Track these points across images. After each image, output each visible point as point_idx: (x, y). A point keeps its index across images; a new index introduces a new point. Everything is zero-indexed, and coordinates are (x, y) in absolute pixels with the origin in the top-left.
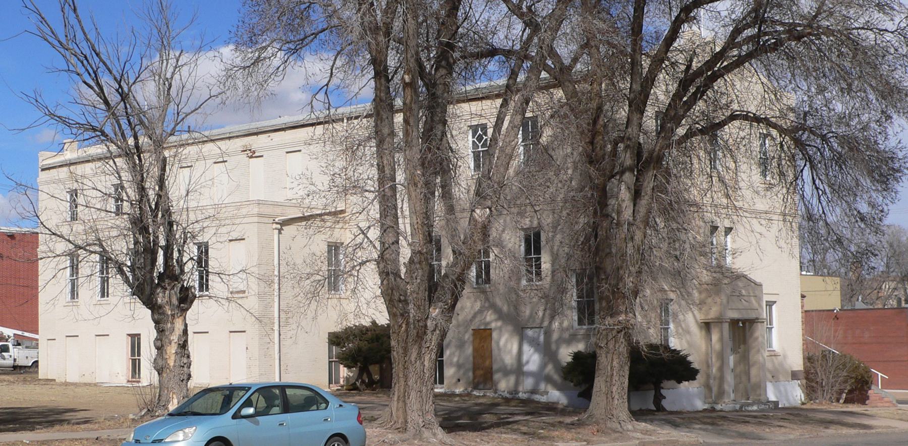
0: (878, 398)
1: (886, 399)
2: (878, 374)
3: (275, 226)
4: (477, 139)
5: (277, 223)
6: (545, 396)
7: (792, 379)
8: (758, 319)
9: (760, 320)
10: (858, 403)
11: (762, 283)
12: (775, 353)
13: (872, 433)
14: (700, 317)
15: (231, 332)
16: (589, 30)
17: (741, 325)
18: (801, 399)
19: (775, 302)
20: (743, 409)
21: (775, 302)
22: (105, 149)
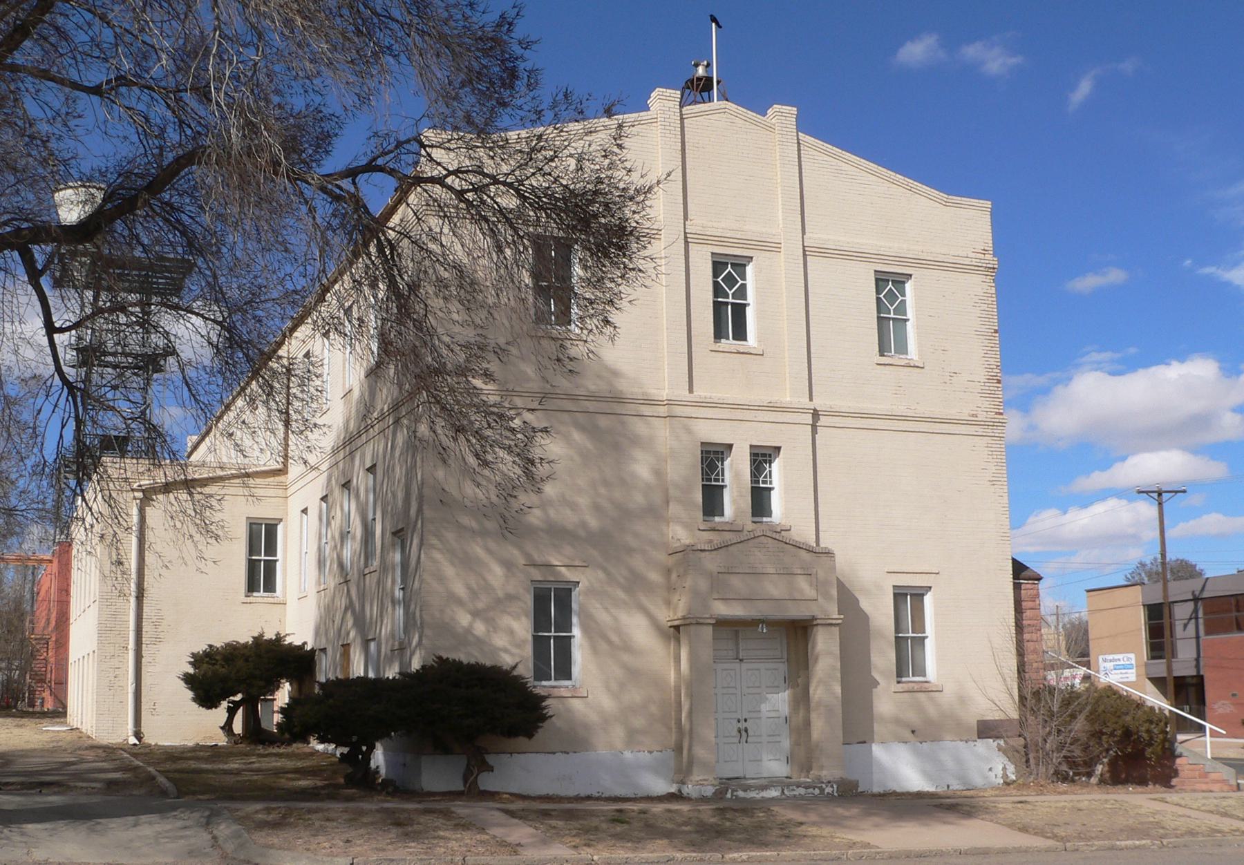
0: (1197, 773)
1: (1213, 776)
2: (1204, 727)
4: (738, 282)
7: (979, 738)
8: (816, 619)
9: (819, 622)
10: (1154, 784)
14: (666, 616)
16: (18, 192)
18: (1005, 776)
20: (729, 796)
21: (930, 588)
22: (658, 172)
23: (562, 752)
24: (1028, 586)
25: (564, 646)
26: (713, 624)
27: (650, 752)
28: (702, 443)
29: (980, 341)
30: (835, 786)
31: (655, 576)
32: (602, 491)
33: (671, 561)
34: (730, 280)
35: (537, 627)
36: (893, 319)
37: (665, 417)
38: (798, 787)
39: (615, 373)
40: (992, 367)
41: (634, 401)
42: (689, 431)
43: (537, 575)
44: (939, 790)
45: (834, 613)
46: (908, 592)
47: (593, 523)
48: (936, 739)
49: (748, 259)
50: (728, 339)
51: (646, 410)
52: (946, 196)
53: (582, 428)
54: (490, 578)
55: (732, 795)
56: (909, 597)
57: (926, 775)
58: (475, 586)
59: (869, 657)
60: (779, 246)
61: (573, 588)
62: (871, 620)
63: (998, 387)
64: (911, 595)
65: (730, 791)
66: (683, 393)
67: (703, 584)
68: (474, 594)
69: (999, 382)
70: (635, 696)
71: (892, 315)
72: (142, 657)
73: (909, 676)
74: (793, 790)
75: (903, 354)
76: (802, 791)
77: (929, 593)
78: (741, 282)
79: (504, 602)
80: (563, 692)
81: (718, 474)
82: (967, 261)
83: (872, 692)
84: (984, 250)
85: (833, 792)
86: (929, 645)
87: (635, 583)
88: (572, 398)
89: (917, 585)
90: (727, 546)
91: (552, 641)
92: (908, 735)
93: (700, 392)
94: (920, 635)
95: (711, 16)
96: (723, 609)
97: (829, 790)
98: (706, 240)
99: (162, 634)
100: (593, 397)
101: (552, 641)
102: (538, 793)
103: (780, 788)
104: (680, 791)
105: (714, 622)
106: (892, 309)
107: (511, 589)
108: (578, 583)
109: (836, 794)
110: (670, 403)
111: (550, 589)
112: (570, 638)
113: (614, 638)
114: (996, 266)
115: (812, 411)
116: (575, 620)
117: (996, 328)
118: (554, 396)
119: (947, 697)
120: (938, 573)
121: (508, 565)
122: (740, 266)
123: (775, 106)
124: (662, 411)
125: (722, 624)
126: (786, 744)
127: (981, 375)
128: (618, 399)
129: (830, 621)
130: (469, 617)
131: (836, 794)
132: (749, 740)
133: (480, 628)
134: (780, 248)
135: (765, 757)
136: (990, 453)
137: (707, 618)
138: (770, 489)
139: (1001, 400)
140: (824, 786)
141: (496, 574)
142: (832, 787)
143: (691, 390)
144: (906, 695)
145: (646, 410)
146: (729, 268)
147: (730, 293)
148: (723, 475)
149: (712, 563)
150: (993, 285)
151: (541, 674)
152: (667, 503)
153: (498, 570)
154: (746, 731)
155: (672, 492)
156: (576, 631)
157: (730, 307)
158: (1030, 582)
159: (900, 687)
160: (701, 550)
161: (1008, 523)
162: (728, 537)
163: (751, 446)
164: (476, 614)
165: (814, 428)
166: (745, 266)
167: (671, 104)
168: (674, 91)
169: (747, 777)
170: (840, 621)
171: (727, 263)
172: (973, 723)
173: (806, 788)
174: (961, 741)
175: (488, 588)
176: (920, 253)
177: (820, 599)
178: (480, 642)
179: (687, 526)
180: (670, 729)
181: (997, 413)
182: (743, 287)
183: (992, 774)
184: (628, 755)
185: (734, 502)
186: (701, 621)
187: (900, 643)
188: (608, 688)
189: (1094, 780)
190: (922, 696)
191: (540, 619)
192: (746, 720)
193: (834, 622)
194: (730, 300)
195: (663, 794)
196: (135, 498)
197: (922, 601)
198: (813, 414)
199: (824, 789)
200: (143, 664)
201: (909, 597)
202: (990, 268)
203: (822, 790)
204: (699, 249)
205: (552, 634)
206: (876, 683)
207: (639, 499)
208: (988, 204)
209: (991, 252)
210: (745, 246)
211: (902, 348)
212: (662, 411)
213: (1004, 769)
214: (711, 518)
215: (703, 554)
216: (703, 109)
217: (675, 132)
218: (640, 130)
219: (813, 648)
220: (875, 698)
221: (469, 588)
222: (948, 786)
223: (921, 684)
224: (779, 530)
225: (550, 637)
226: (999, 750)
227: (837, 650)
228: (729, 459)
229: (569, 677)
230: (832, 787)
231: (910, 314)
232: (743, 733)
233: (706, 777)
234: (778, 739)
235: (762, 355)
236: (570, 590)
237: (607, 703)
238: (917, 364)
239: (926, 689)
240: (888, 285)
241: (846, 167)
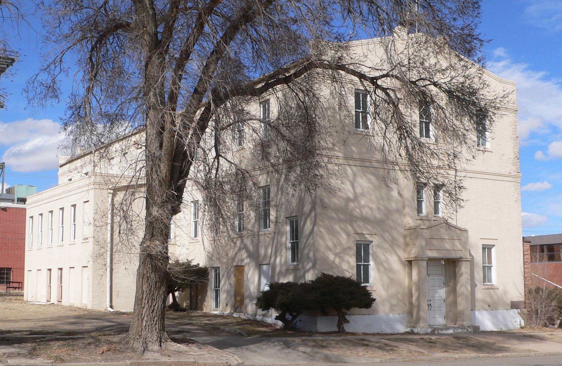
3: (109, 191)
5: (110, 189)
6: (270, 319)
7: (511, 308)
8: (462, 258)
9: (463, 259)
11: (467, 229)
12: (493, 286)
13: (498, 357)
14: (404, 256)
15: (84, 267)
17: (443, 263)
18: (520, 324)
19: (494, 245)
20: (436, 332)
21: (494, 245)
25: (366, 268)
27: (399, 314)
32: (381, 202)
33: (405, 233)
47: (378, 216)
53: (373, 174)
54: (341, 239)
57: (494, 324)
58: (335, 242)
64: (488, 248)
67: (423, 243)
68: (335, 246)
69: (518, 159)
70: (393, 291)
77: (494, 248)
79: (345, 250)
86: (494, 270)
87: (393, 243)
91: (362, 266)
92: (487, 307)
97: (470, 330)
101: (362, 266)
104: (412, 331)
105: (427, 259)
108: (372, 241)
111: (361, 244)
112: (368, 265)
113: (386, 265)
116: (371, 258)
119: (500, 292)
121: (348, 235)
125: (431, 260)
126: (444, 310)
127: (512, 156)
130: (333, 256)
132: (432, 309)
133: (337, 261)
135: (437, 316)
137: (277, 240)
144: (486, 290)
149: (426, 233)
152: (404, 207)
153: (344, 236)
154: (430, 305)
155: (407, 203)
156: (372, 263)
164: (336, 255)
175: (341, 244)
177: (463, 250)
178: (338, 267)
179: (412, 217)
180: (405, 304)
184: (391, 315)
185: (427, 207)
186: (423, 259)
188: (383, 286)
189: (556, 326)
190: (491, 291)
191: (358, 259)
192: (430, 301)
193: (468, 259)
196: (110, 193)
203: (467, 330)
205: (363, 263)
213: (520, 321)
219: (459, 270)
220: (476, 291)
221: (334, 243)
225: (361, 265)
227: (469, 271)
234: (441, 309)
236: (369, 245)
239: (493, 288)
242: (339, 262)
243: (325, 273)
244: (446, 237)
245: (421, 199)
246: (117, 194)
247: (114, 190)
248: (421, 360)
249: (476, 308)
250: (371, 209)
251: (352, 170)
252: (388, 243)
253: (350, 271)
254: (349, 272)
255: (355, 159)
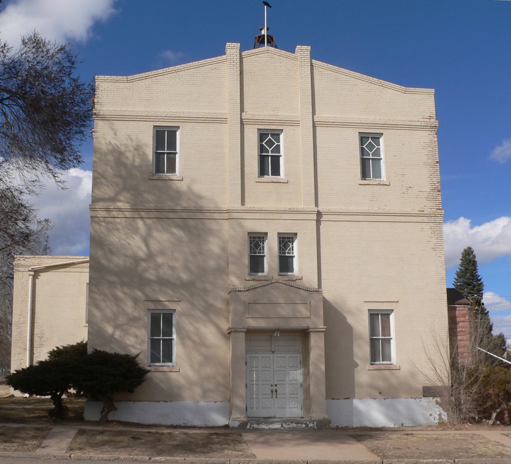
14: (225, 326)
18: (440, 418)
20: (248, 427)
21: (393, 310)
23: (163, 401)
24: (461, 309)
25: (168, 344)
26: (245, 332)
28: (249, 233)
29: (428, 168)
30: (315, 423)
31: (219, 304)
34: (270, 143)
35: (152, 334)
36: (372, 159)
37: (228, 219)
38: (292, 423)
39: (200, 197)
40: (434, 183)
41: (209, 211)
42: (241, 226)
43: (151, 306)
44: (396, 426)
45: (321, 326)
46: (380, 313)
47: (184, 276)
48: (395, 396)
49: (177, 128)
50: (268, 175)
51: (217, 216)
52: (405, 88)
55: (250, 427)
56: (380, 316)
57: (389, 417)
59: (353, 350)
60: (226, 120)
61: (173, 312)
62: (354, 329)
63: (438, 194)
64: (381, 315)
65: (249, 424)
66: (238, 205)
67: (240, 308)
70: (209, 370)
71: (371, 157)
72: (34, 354)
73: (380, 361)
74: (289, 425)
75: (378, 178)
76: (294, 425)
77: (393, 314)
78: (276, 144)
80: (165, 369)
81: (260, 250)
82: (419, 124)
83: (354, 370)
84: (430, 117)
85: (314, 426)
86: (393, 343)
88: (173, 211)
89: (384, 309)
90: (255, 288)
91: (161, 341)
92: (377, 394)
93: (249, 205)
94: (387, 337)
95: (264, 2)
96: (253, 323)
97: (311, 425)
98: (254, 122)
99: (44, 342)
100: (186, 210)
101: (161, 341)
102: (149, 423)
103: (280, 423)
106: (371, 153)
107: (136, 314)
109: (316, 427)
110: (228, 211)
111: (161, 313)
113: (195, 338)
114: (437, 125)
115: (316, 213)
116: (174, 330)
117: (438, 160)
118: (163, 211)
120: (398, 302)
121: (136, 301)
122: (276, 135)
123: (297, 46)
124: (226, 216)
125: (250, 332)
127: (427, 188)
128: (201, 211)
129: (318, 330)
131: (316, 427)
132: (278, 396)
133: (118, 334)
134: (299, 123)
136: (433, 232)
138: (293, 257)
139: (440, 201)
140: (308, 423)
141: (129, 307)
142: (313, 423)
143: (243, 203)
145: (217, 216)
146: (270, 137)
147: (270, 150)
148: (293, 250)
150: (436, 136)
151: (154, 359)
152: (228, 265)
154: (276, 391)
155: (230, 259)
156: (174, 336)
157: (270, 158)
158: (462, 306)
159: (372, 367)
160: (239, 291)
161: (445, 272)
162: (265, 283)
163: (278, 233)
164: (117, 327)
165: (318, 222)
166: (279, 135)
167: (235, 51)
168: (236, 44)
169: (277, 417)
170: (324, 330)
171: (268, 134)
172: (420, 387)
173: (297, 423)
174: (412, 398)
176: (388, 121)
177: (312, 317)
179: (239, 277)
181: (437, 209)
182: (278, 147)
183: (432, 418)
184: (202, 403)
187: (373, 342)
191: (154, 329)
192: (276, 385)
193: (320, 330)
194: (270, 154)
195: (222, 425)
196: (30, 275)
197: (389, 318)
198: (317, 214)
199: (308, 425)
200: (34, 357)
201: (380, 316)
202: (433, 127)
203: (307, 425)
204: (249, 127)
206: (357, 365)
207: (212, 263)
208: (433, 91)
209: (435, 118)
210: (277, 124)
211: (377, 174)
212: (226, 216)
213: (440, 415)
214: (256, 274)
215: (240, 293)
216: (254, 52)
217: (236, 66)
218: (217, 66)
220: (355, 373)
222: (402, 424)
223: (386, 366)
224: (295, 280)
226: (437, 404)
227: (323, 345)
228: (267, 241)
229: (171, 361)
230: (313, 423)
231: (382, 155)
232: (274, 393)
233: (239, 416)
235: (288, 183)
236: (172, 314)
237: (192, 375)
238: (385, 183)
239: (390, 369)
240: (369, 140)
241: (342, 76)
242: (120, 336)
243: (99, 349)
244: (281, 301)
245: (291, 255)
246: (40, 276)
247: (35, 271)
248: (102, 460)
249: (356, 395)
250: (173, 268)
251: (145, 224)
252: (199, 310)
253: (138, 346)
254: (135, 348)
255: (148, 210)
